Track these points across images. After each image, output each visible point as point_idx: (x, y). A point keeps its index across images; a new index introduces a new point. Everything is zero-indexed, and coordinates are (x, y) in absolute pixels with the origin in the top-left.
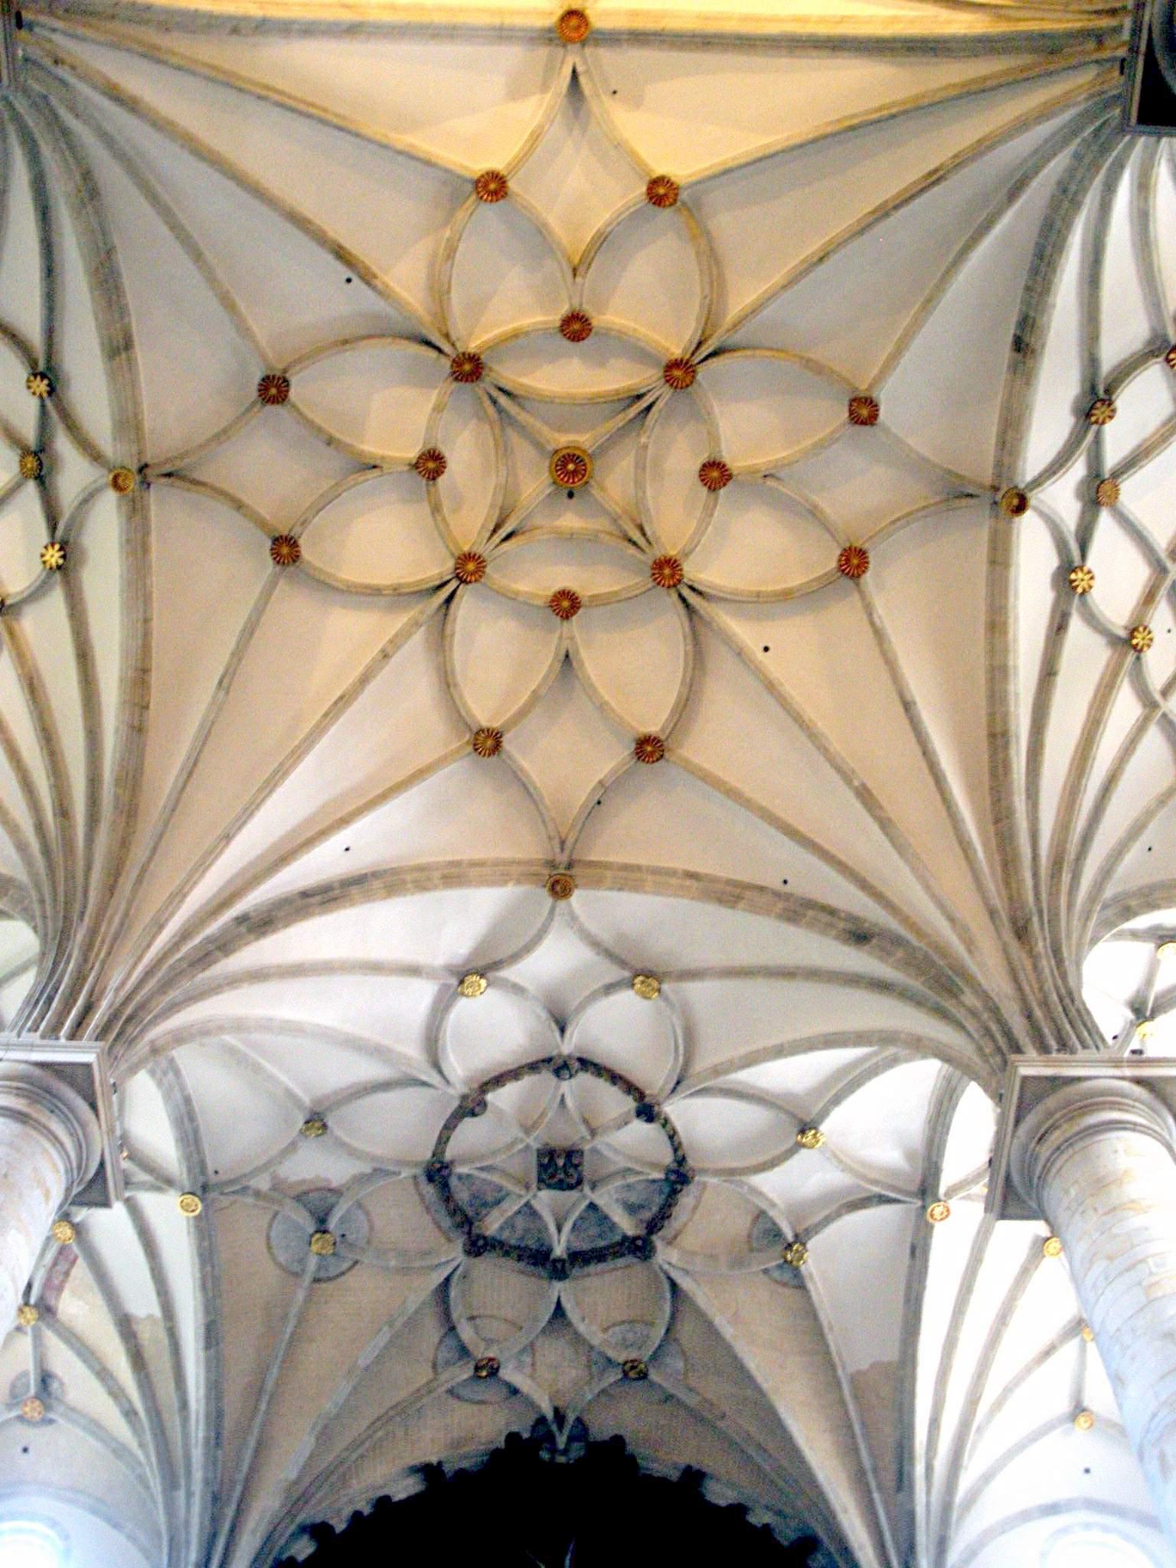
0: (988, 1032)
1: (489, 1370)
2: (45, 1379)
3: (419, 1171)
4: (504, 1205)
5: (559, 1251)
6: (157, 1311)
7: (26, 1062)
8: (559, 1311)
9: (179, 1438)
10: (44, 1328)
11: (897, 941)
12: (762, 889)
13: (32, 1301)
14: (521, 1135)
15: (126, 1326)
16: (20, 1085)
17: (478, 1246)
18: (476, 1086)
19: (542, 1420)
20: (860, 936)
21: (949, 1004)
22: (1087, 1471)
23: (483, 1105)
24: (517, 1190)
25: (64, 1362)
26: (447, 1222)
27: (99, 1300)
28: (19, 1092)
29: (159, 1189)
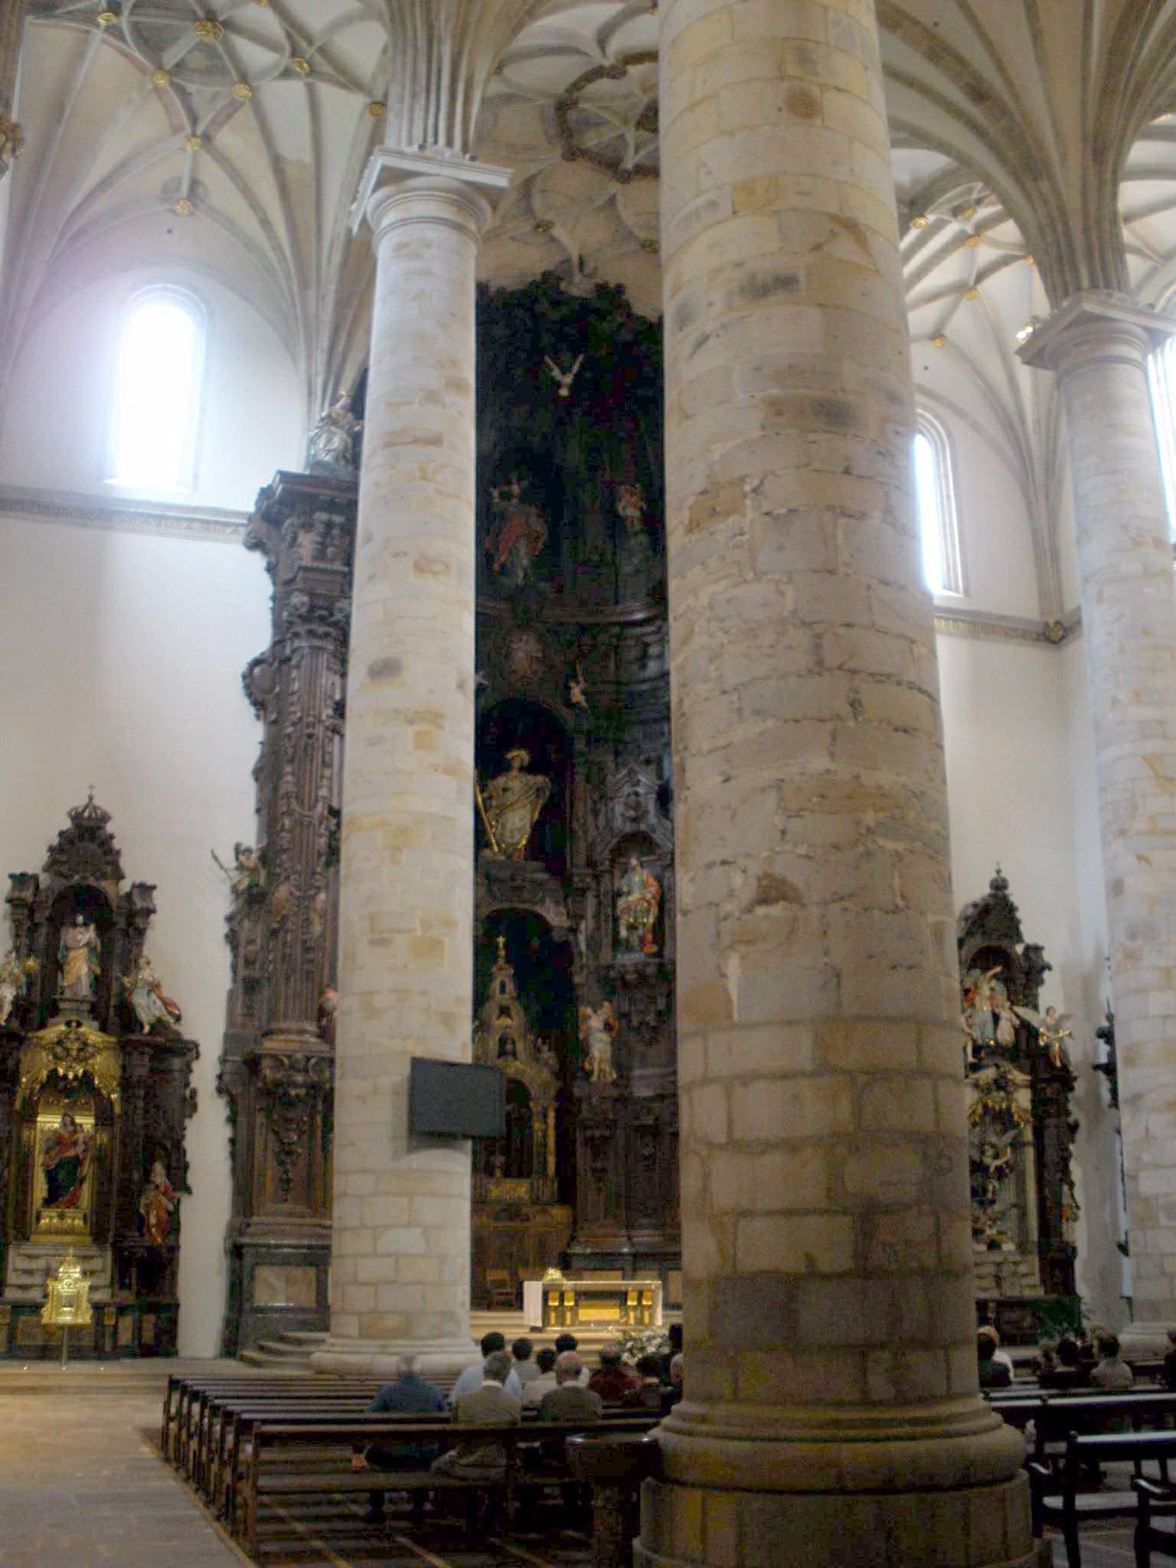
0: (1057, 242)
1: (543, 227)
2: (195, 183)
3: (552, 102)
4: (604, 129)
5: (629, 164)
6: (308, 158)
7: (458, 180)
8: (612, 200)
9: (314, 260)
10: (203, 152)
11: (1004, 111)
12: (916, 23)
13: (199, 132)
14: (637, 91)
15: (277, 164)
16: (454, 197)
17: (573, 154)
18: (620, 57)
19: (567, 261)
20: (979, 94)
21: (1029, 184)
22: (926, 368)
23: (624, 73)
24: (617, 123)
25: (213, 175)
26: (553, 131)
27: (256, 138)
28: (452, 203)
29: (344, 86)
